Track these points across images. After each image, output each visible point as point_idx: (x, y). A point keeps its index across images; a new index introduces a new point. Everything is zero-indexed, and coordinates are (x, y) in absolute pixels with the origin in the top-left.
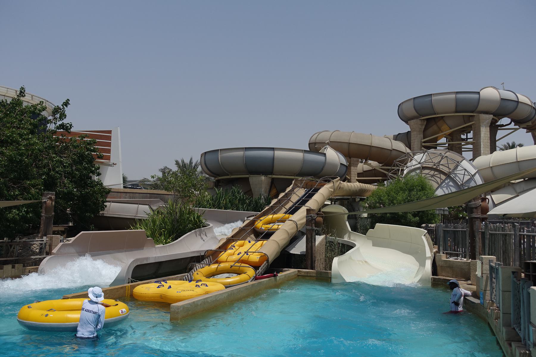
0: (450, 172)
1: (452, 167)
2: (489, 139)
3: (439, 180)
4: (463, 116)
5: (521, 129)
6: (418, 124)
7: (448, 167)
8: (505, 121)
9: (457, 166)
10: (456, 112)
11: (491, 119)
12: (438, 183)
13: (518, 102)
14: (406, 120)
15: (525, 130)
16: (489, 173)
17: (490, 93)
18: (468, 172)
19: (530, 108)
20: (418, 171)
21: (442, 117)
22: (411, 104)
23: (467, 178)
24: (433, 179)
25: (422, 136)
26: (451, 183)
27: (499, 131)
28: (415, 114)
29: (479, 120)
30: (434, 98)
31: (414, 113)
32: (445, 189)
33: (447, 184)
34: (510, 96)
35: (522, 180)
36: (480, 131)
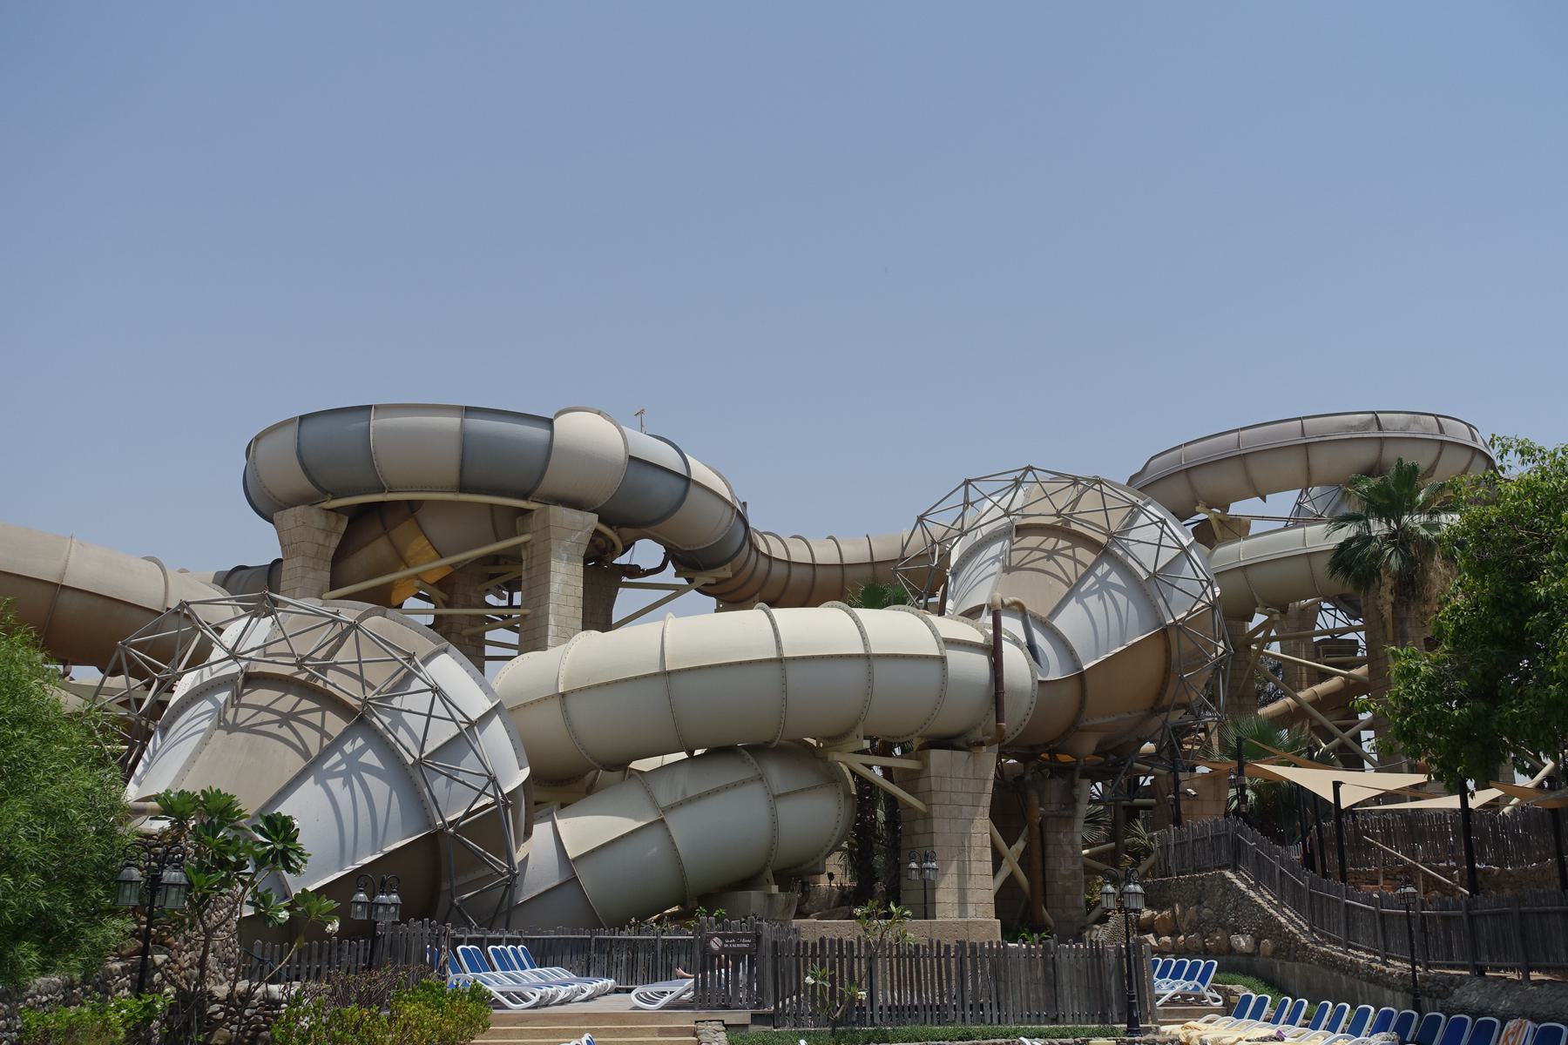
0: (366, 702)
1: (379, 676)
2: (580, 603)
3: (313, 741)
4: (492, 505)
5: (693, 594)
6: (317, 528)
7: (360, 678)
8: (647, 553)
9: (402, 685)
10: (463, 488)
11: (590, 529)
12: (305, 753)
13: (687, 480)
14: (266, 504)
15: (713, 601)
16: (548, 721)
17: (590, 431)
18: (445, 699)
19: (728, 512)
20: (222, 697)
21: (410, 504)
22: (289, 437)
23: (442, 732)
24: (285, 732)
25: (326, 576)
26: (370, 758)
27: (623, 593)
28: (302, 484)
29: (547, 527)
30: (376, 422)
31: (302, 484)
32: (335, 784)
33: (347, 759)
34: (666, 456)
35: (683, 755)
36: (547, 572)
